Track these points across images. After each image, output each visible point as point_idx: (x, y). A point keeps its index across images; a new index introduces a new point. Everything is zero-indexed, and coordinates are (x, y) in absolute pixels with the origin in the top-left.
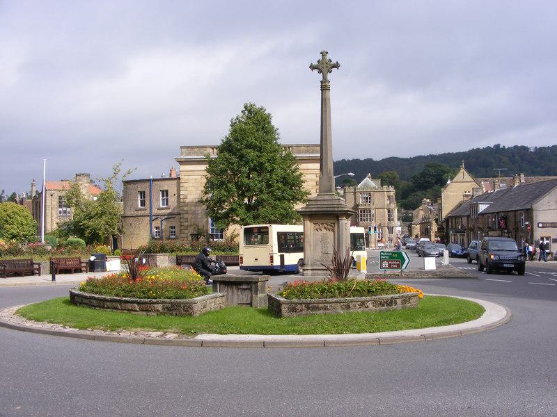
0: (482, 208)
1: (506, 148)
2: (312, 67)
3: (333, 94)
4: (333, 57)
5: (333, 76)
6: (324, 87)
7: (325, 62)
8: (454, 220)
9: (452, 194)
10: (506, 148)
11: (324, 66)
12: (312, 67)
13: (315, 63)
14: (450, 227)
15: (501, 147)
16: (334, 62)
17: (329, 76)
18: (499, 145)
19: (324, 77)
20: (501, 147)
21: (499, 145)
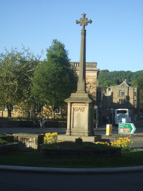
6: (84, 33)
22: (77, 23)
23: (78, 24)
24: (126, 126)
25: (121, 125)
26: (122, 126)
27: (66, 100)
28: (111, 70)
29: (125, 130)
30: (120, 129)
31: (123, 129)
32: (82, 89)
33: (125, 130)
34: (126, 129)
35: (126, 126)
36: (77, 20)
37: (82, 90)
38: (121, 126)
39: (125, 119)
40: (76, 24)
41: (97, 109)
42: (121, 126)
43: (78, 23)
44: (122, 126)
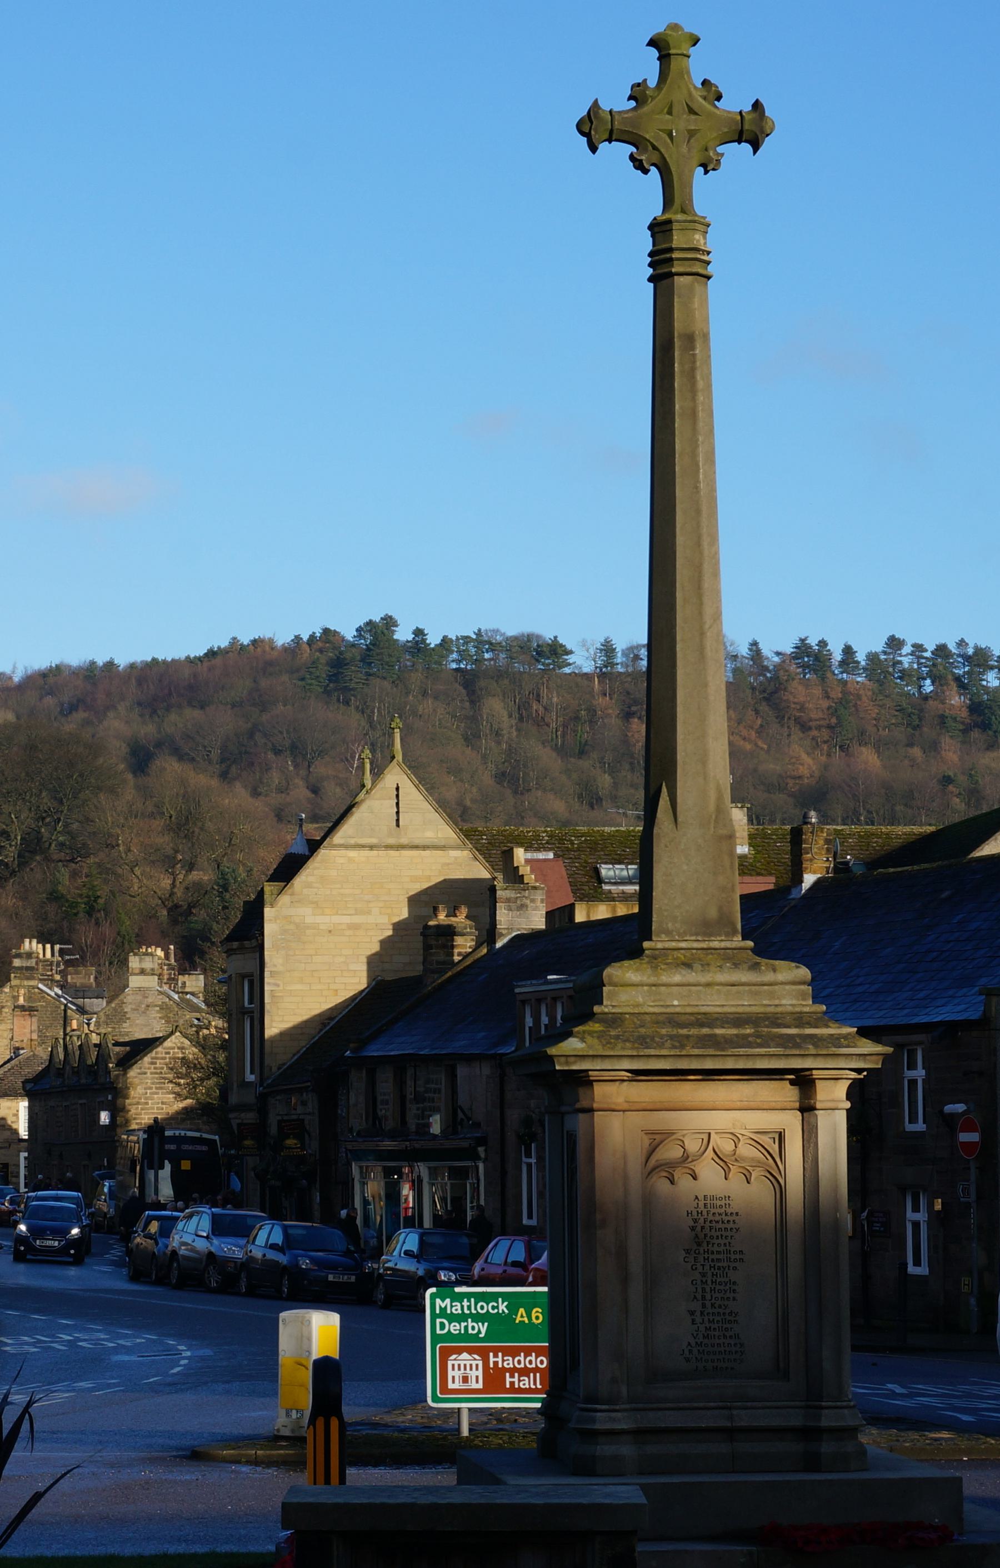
0: (104, 1117)
1: (433, 640)
2: (594, 128)
3: (727, 312)
4: (730, 70)
5: (725, 193)
6: (671, 262)
7: (679, 97)
8: (386, 1085)
9: (324, 921)
10: (433, 640)
11: (667, 127)
12: (594, 128)
13: (617, 101)
14: (410, 1096)
15: (403, 634)
16: (735, 102)
17: (704, 191)
18: (389, 622)
19: (671, 193)
20: (403, 634)
21: (389, 622)
22: (652, 43)
23: (654, 53)
24: (521, 1316)
25: (457, 1309)
26: (461, 1318)
27: (572, 1050)
28: (122, 661)
29: (509, 1363)
30: (446, 1354)
31: (483, 1353)
32: (713, 913)
33: (509, 1363)
34: (513, 1352)
35: (521, 1316)
36: (696, 41)
37: (707, 928)
38: (455, 1328)
39: (183, 1168)
40: (658, 28)
41: (433, 1164)
42: (455, 1328)
43: (664, 58)
44: (461, 1318)
